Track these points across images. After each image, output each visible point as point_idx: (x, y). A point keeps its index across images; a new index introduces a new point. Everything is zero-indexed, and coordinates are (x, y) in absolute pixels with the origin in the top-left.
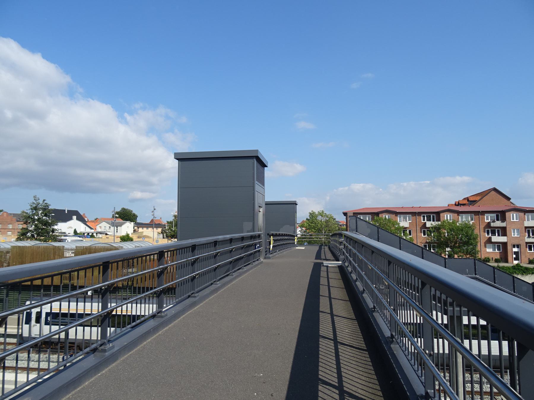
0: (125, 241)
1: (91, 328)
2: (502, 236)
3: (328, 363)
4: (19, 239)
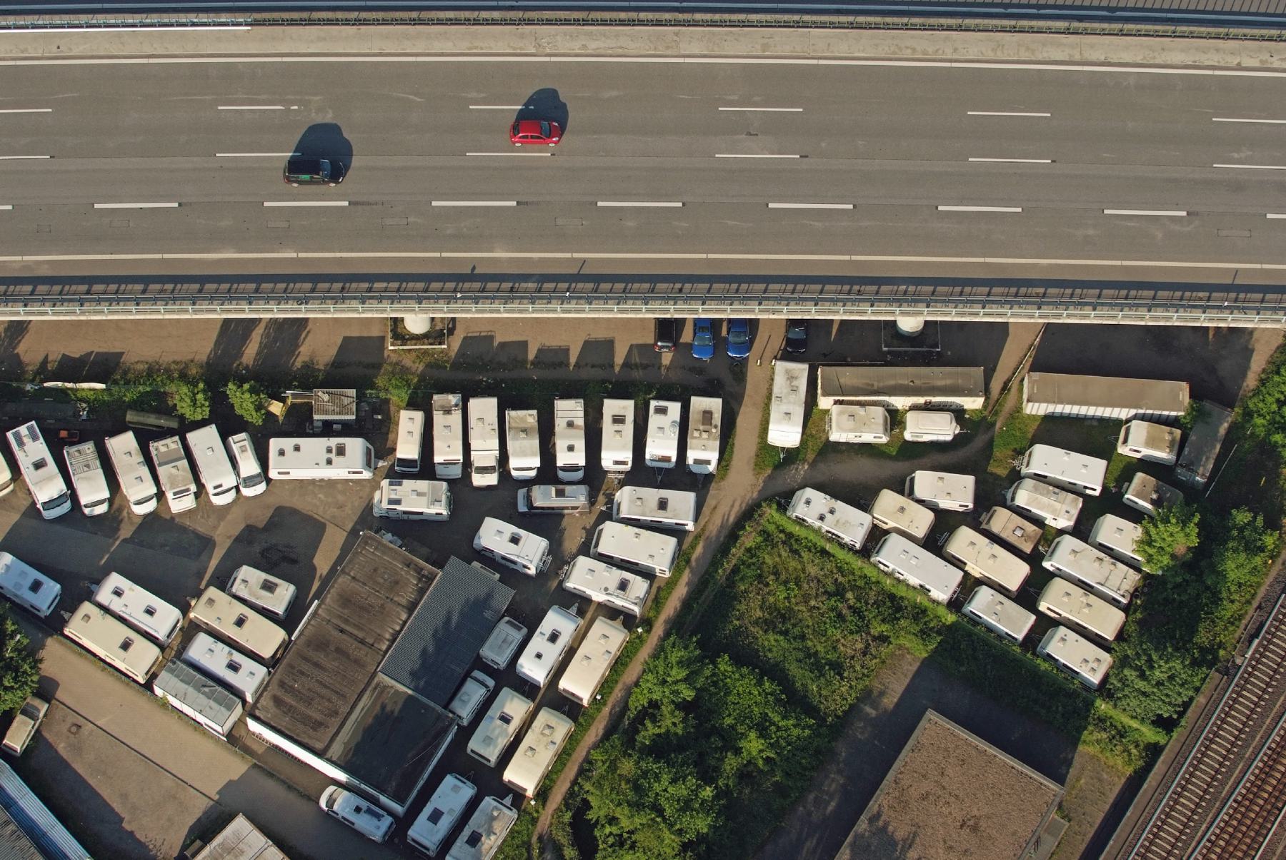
3: (663, 505)
4: (295, 152)
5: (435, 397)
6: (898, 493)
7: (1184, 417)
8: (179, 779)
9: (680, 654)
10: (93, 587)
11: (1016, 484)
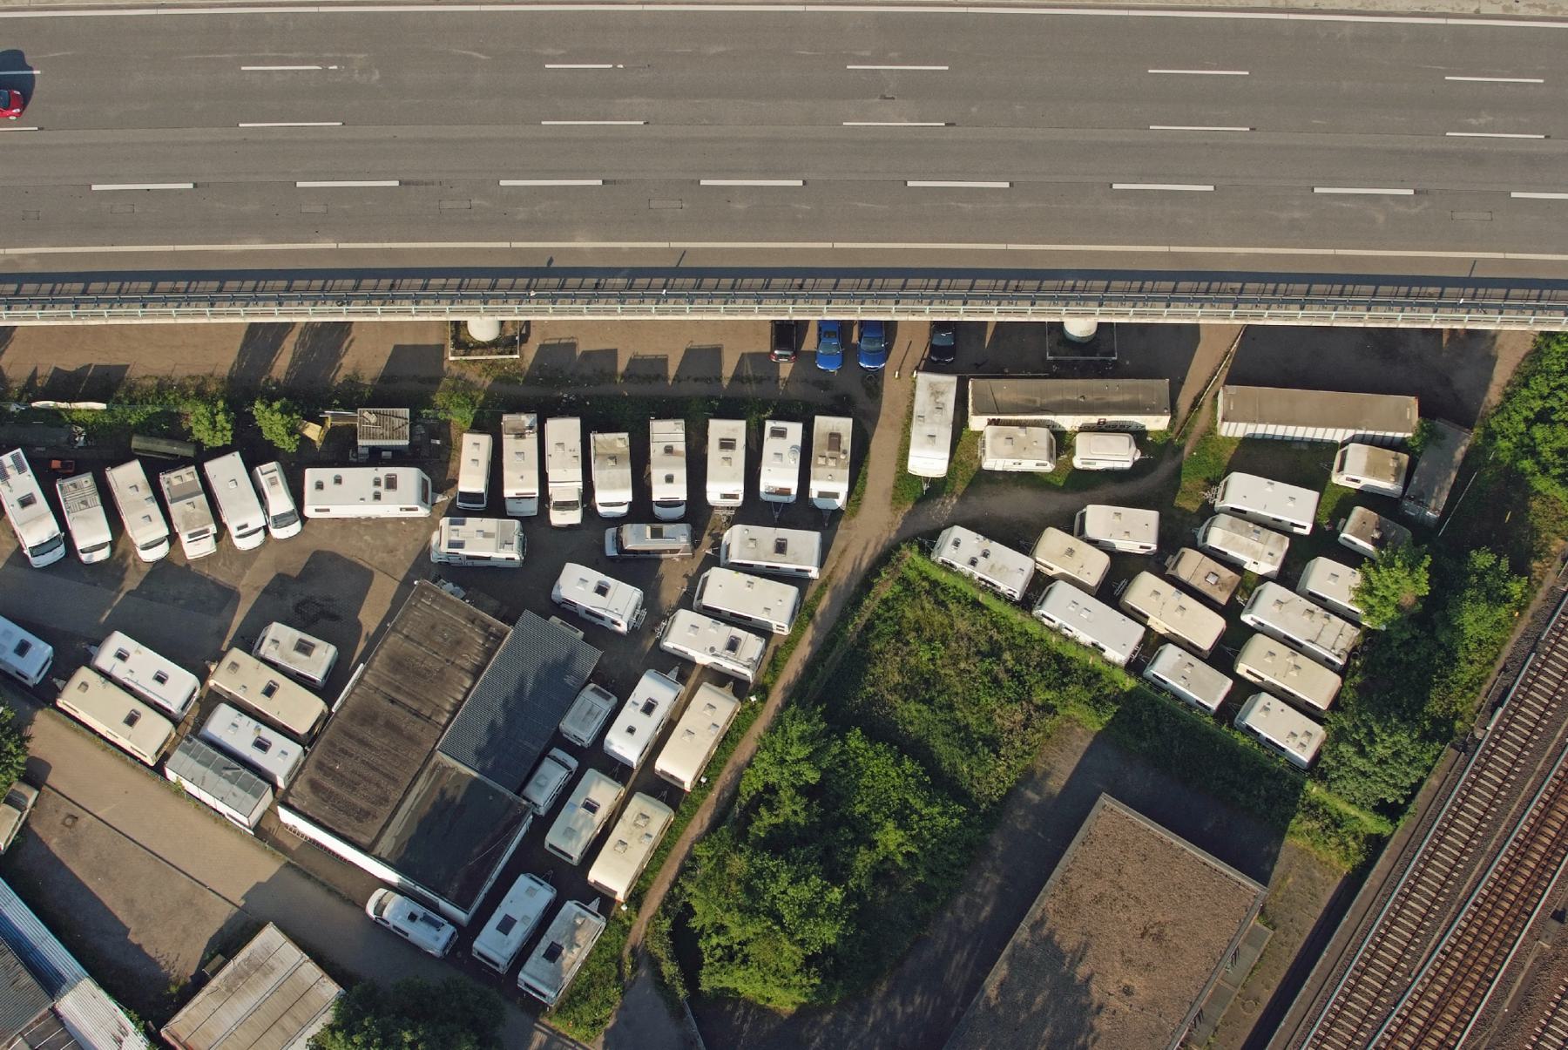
0: (151, 436)
3: (781, 547)
5: (505, 418)
7: (1413, 439)
8: (197, 881)
9: (802, 727)
10: (93, 649)
11: (1209, 521)
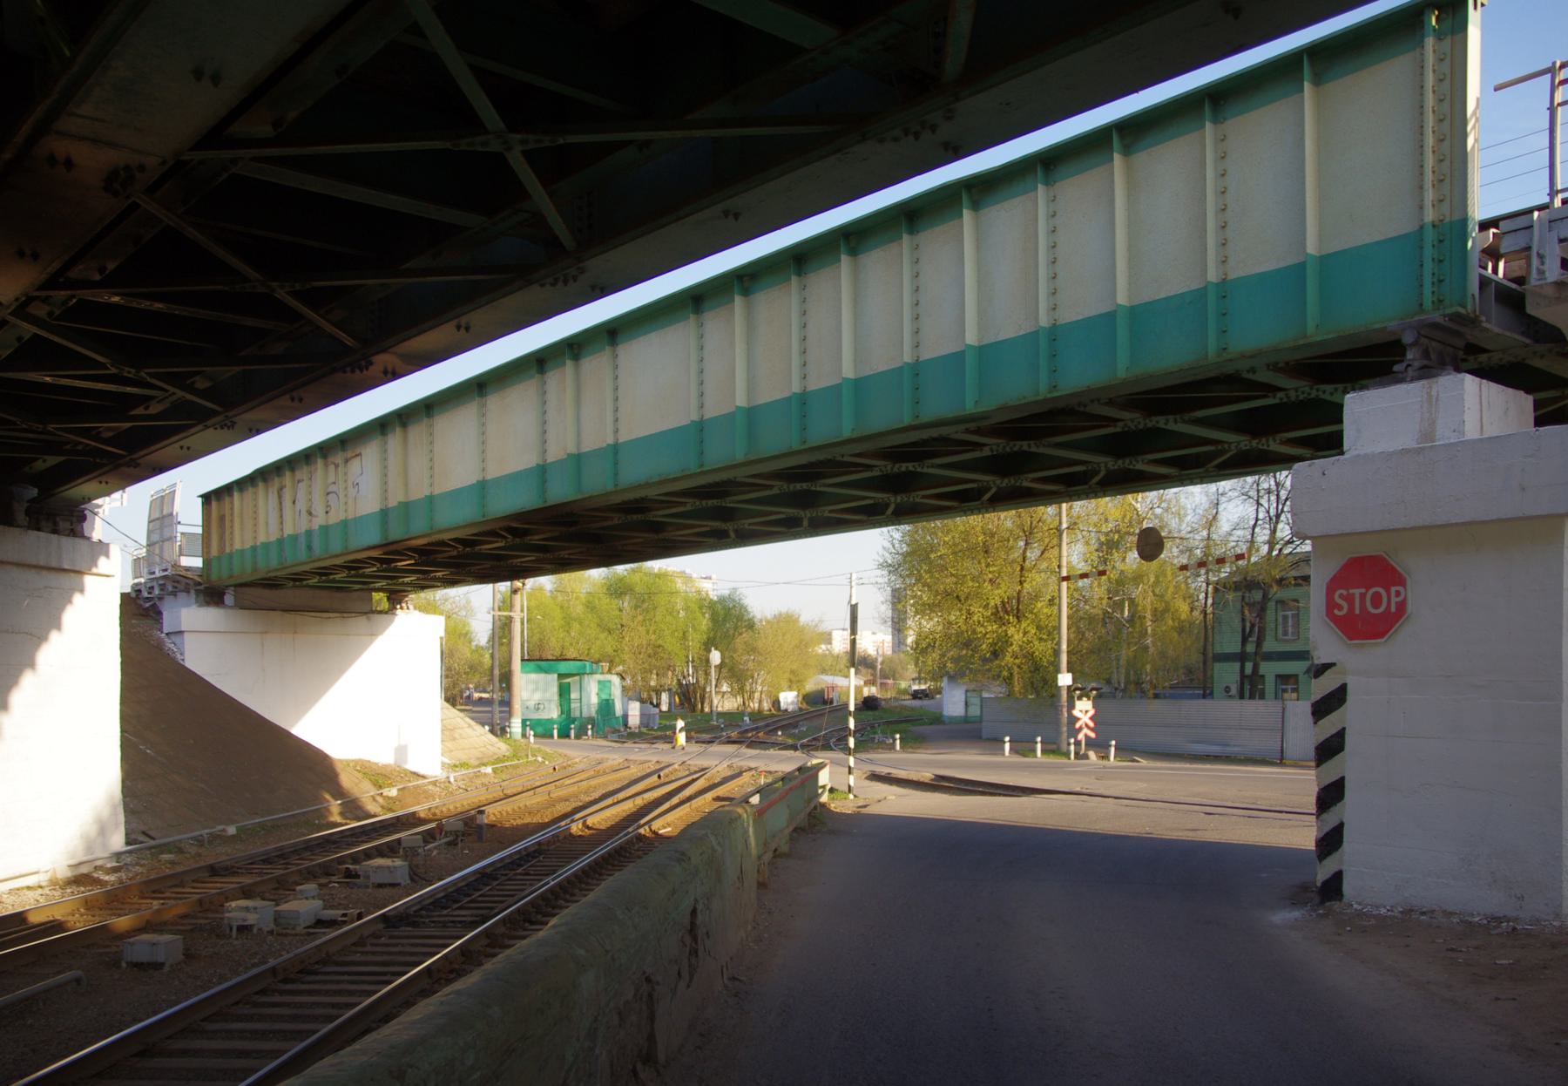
1: (327, 521)
2: (1341, 421)
3: (643, 799)
6: (1343, 787)
